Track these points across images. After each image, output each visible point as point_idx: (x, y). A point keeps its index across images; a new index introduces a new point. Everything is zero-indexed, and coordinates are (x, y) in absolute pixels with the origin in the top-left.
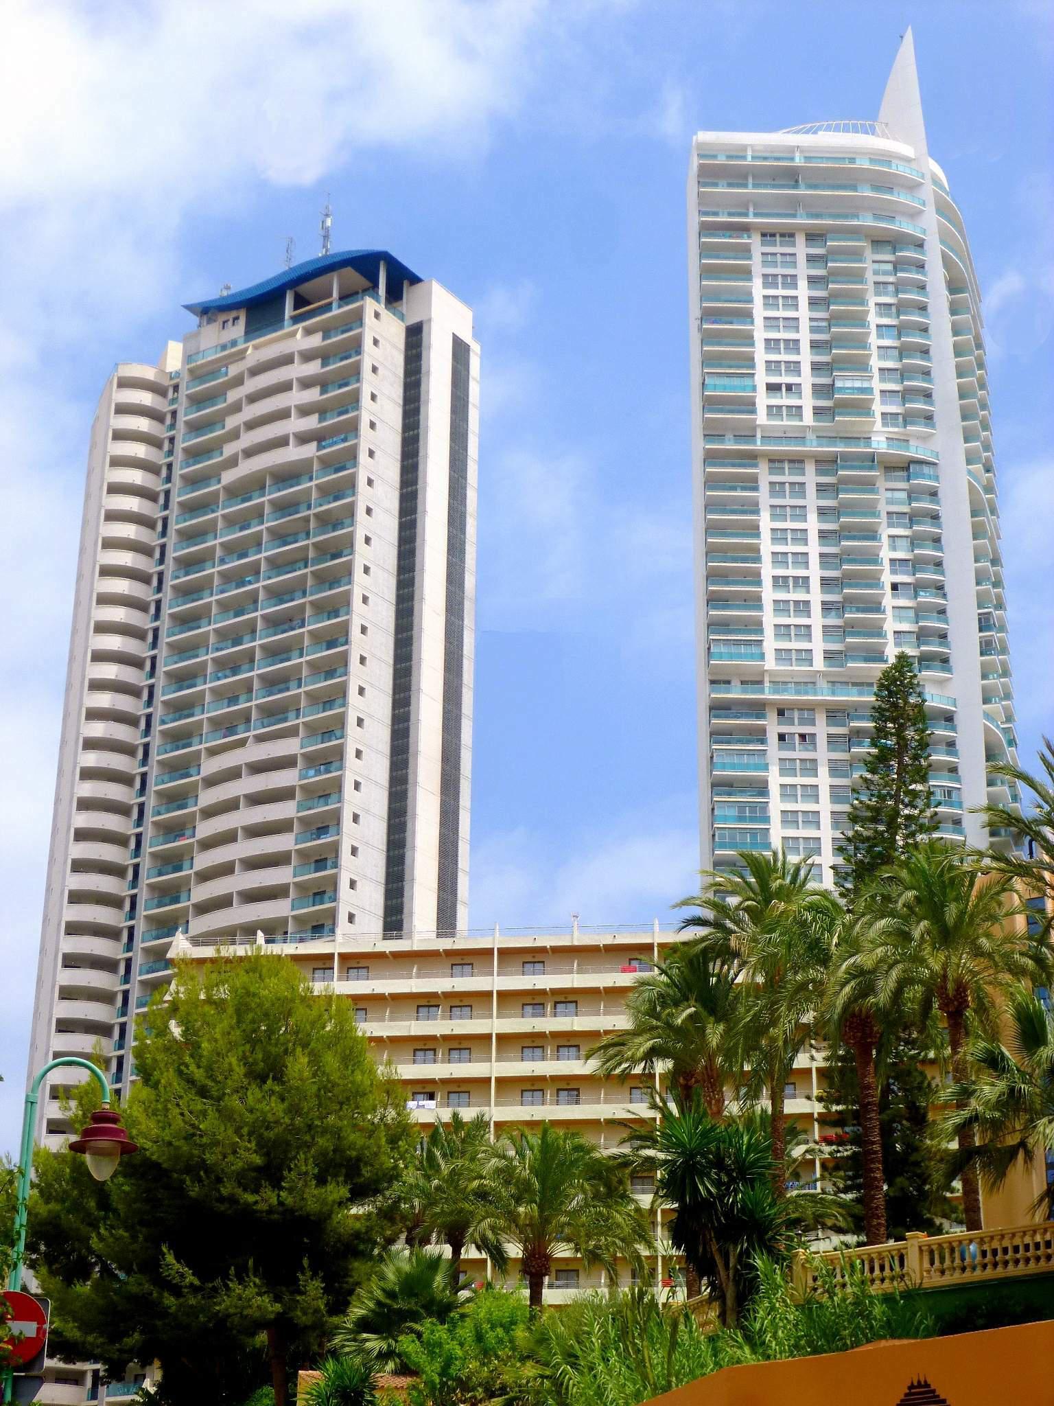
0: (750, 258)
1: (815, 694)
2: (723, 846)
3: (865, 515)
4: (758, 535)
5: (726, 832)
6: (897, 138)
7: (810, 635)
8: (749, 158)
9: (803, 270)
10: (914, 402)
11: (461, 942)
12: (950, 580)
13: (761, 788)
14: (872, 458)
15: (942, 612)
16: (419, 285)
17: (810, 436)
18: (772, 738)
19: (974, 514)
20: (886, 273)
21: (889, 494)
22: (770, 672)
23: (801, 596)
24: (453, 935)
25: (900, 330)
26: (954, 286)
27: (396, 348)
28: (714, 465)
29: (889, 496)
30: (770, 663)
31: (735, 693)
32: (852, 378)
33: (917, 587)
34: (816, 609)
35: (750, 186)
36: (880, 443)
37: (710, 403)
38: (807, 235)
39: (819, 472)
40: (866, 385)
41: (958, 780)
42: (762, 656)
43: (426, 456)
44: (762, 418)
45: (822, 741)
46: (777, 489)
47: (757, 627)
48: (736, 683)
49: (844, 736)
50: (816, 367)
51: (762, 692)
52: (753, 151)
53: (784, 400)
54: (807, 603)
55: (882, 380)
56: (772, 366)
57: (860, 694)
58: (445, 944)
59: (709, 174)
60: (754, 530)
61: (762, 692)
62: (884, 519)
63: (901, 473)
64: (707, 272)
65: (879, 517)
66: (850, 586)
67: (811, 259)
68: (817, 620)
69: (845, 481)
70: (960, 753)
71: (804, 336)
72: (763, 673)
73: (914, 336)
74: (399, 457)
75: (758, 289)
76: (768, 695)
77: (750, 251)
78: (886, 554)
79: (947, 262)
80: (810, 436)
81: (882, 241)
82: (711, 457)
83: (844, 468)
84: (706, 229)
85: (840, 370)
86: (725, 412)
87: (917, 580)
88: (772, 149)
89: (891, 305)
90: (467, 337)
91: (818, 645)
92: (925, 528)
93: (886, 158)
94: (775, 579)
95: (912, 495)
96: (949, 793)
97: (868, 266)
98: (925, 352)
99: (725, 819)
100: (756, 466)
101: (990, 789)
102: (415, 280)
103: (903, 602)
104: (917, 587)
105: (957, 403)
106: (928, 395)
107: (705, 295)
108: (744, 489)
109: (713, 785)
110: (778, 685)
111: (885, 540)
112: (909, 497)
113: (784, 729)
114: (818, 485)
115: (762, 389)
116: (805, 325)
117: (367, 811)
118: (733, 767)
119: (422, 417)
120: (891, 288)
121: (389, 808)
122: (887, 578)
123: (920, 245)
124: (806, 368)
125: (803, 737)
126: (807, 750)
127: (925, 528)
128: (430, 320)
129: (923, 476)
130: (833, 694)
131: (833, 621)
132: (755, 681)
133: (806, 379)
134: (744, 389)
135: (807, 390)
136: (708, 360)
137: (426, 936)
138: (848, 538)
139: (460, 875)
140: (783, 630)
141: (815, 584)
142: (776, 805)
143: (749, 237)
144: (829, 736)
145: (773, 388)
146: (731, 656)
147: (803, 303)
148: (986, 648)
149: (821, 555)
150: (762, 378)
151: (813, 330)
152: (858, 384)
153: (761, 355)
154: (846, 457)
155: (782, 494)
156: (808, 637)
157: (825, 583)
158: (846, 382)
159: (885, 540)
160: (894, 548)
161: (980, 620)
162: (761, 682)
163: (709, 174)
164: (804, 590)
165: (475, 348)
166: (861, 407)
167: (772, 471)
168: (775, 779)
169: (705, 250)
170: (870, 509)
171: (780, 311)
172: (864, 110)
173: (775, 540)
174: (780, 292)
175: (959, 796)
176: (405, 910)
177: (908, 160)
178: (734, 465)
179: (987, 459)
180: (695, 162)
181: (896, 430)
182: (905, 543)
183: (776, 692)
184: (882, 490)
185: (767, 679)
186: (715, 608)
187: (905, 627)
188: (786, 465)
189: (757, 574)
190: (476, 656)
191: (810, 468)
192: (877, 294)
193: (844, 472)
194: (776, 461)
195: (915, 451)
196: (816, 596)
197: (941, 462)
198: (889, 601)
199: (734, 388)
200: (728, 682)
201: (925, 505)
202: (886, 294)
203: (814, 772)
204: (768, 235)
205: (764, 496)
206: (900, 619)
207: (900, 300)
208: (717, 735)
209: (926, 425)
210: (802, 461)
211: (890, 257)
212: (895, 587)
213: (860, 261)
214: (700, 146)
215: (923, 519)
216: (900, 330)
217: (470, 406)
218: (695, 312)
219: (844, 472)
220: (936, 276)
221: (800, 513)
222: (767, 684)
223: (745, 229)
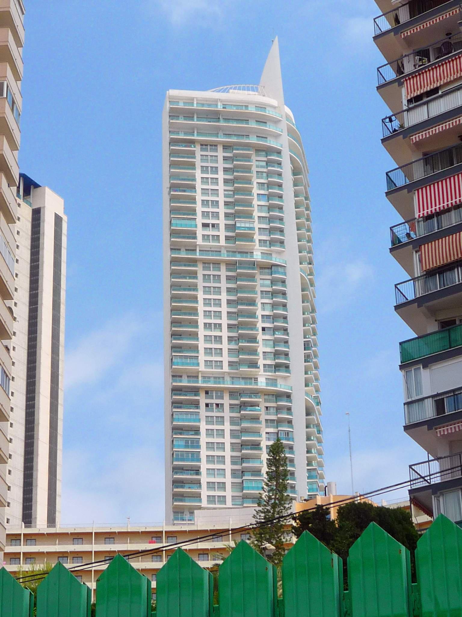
0: (195, 158)
1: (224, 384)
2: (177, 460)
3: (249, 292)
4: (197, 302)
5: (179, 453)
6: (268, 96)
7: (225, 501)
8: (195, 105)
9: (221, 165)
10: (275, 236)
11: (58, 529)
12: (289, 290)
13: (196, 431)
14: (253, 263)
15: (286, 342)
16: (39, 189)
17: (224, 251)
18: (202, 406)
19: (303, 290)
20: (262, 167)
21: (262, 282)
22: (203, 372)
23: (218, 333)
24: (55, 527)
25: (269, 197)
26: (296, 172)
27: (28, 221)
28: (175, 168)
29: (262, 283)
30: (202, 368)
31: (185, 383)
33: (275, 329)
34: (225, 340)
36: (257, 256)
37: (174, 233)
38: (223, 146)
39: (228, 270)
40: (251, 226)
41: (292, 428)
42: (198, 364)
43: (40, 348)
44: (199, 241)
45: (227, 408)
46: (206, 278)
47: (195, 348)
48: (183, 250)
49: (238, 405)
50: (227, 215)
51: (198, 382)
52: (197, 100)
53: (210, 232)
54: (220, 337)
55: (260, 223)
56: (205, 214)
57: (246, 384)
58: (52, 530)
59: (174, 114)
60: (195, 299)
61: (198, 382)
62: (259, 295)
63: (267, 271)
64: (173, 165)
65: (252, 173)
66: (242, 329)
67: (225, 159)
68: (225, 346)
69: (240, 275)
70: (291, 372)
71: (221, 199)
72: (198, 372)
73: (275, 200)
74: (29, 276)
75: (199, 174)
76: (200, 384)
77: (194, 154)
78: (260, 312)
79: (292, 160)
80: (224, 251)
81: (259, 150)
82: (174, 261)
83: (240, 268)
84: (173, 142)
85: (239, 217)
86: (181, 238)
87: (275, 326)
88: (206, 100)
89: (274, 420)
90: (61, 214)
91: (225, 358)
92: (279, 299)
93: (262, 107)
94: (204, 236)
95: (273, 282)
96: (288, 433)
97: (254, 163)
98: (281, 208)
99: (179, 446)
100: (196, 266)
101: (308, 430)
102: (37, 186)
103: (267, 337)
104: (275, 329)
105: (300, 293)
106: (281, 231)
107: (172, 176)
108: (190, 278)
109: (172, 348)
110: (206, 378)
111: (259, 305)
112: (272, 283)
113: (209, 401)
114: (224, 179)
115: (200, 226)
116: (221, 193)
117: (15, 452)
118: (183, 420)
119: (34, 464)
120: (265, 175)
121: (24, 482)
122: (260, 325)
123: (279, 152)
124: (222, 216)
125: (217, 405)
126: (220, 412)
127: (279, 299)
128: (44, 207)
129: (279, 273)
130: (233, 384)
131: (233, 346)
132: (194, 376)
133: (222, 222)
134: (191, 226)
135: (222, 227)
136: (173, 210)
137: (42, 527)
138: (242, 305)
139: (59, 436)
140: (210, 419)
141: (225, 327)
142: (204, 439)
143: (195, 147)
144: (230, 405)
145: (205, 225)
146: (183, 364)
147: (221, 182)
148: (307, 358)
149: (228, 313)
150: (200, 220)
151: (226, 196)
152: (247, 225)
153: (199, 208)
154: (241, 262)
155: (207, 160)
156: (221, 354)
157: (230, 327)
158: (242, 224)
159: (259, 305)
160: (263, 309)
161: (305, 344)
162: (197, 377)
163: (174, 114)
164: (219, 330)
165: (65, 218)
166: (249, 238)
167: (204, 268)
168: (203, 427)
169: (173, 153)
170: (252, 289)
171: (210, 186)
172: (251, 78)
173: (205, 304)
174: (210, 176)
175: (293, 435)
176: (33, 500)
177: (275, 108)
178: (185, 266)
179: (308, 215)
180: (168, 106)
181: (270, 374)
182: (269, 307)
183: (204, 382)
184: (258, 280)
185: (200, 375)
186: (175, 339)
187: (268, 350)
188: (211, 266)
189: (196, 322)
190: (66, 316)
191: (223, 267)
192: (258, 178)
193: (241, 271)
194: (206, 264)
195: (276, 260)
196: (225, 333)
197: (288, 266)
198: (261, 337)
199: (186, 226)
200: (180, 250)
201: (279, 288)
202: (262, 178)
203: (223, 423)
204: (204, 145)
205: (200, 282)
206: (266, 346)
207: (269, 181)
208: (176, 404)
209: (281, 247)
210: (219, 264)
211: (265, 159)
212: (264, 329)
213: (249, 161)
214: (170, 97)
215: (278, 294)
216: (269, 197)
217: (63, 235)
218: (166, 184)
219: (241, 271)
220: (287, 169)
221: (218, 290)
222: (200, 378)
223: (194, 262)
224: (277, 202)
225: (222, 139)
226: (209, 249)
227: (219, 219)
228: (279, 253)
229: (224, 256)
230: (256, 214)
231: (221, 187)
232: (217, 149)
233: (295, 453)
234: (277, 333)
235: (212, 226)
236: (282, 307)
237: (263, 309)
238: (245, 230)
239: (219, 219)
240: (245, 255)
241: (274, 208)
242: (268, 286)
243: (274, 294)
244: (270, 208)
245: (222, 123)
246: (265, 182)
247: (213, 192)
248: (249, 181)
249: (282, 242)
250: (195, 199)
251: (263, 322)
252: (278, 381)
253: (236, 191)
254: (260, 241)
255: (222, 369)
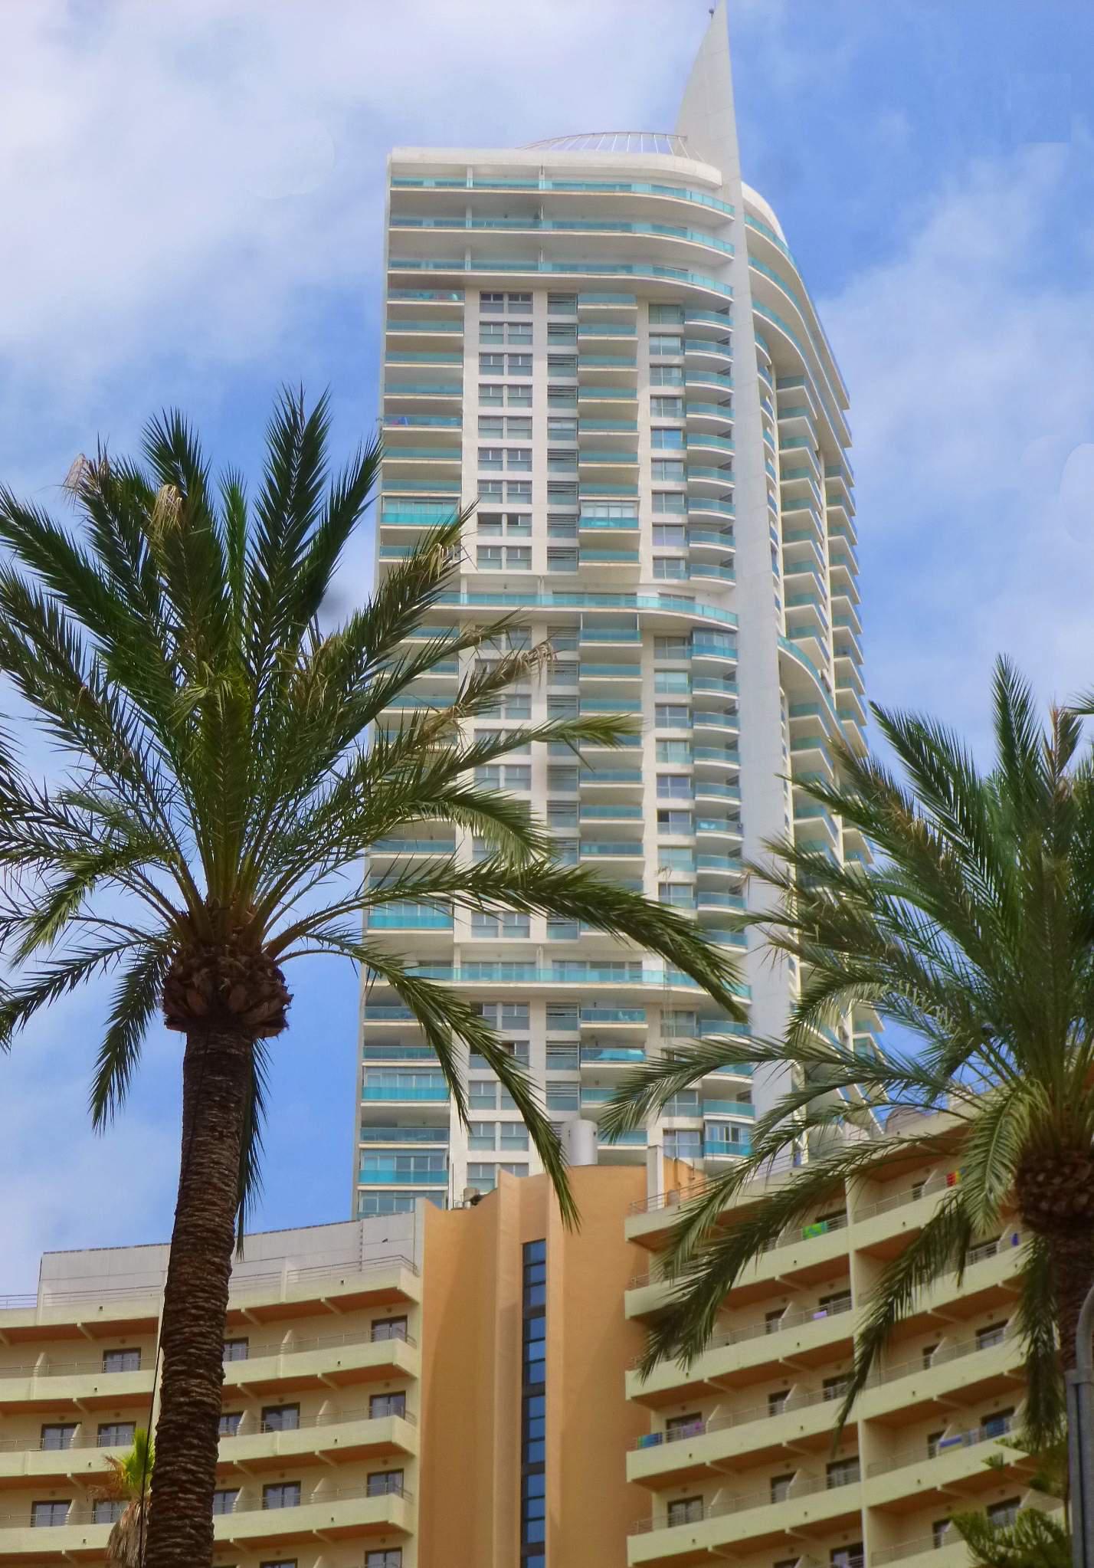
8: (469, 184)
9: (541, 347)
14: (630, 621)
20: (669, 351)
22: (465, 948)
29: (658, 681)
32: (608, 505)
33: (700, 815)
35: (469, 223)
38: (550, 296)
40: (629, 514)
50: (556, 490)
53: (504, 537)
67: (554, 330)
71: (540, 444)
75: (472, 374)
79: (762, 332)
89: (678, 559)
96: (735, 1132)
104: (700, 815)
116: (540, 426)
122: (652, 802)
123: (723, 310)
129: (712, 650)
130: (562, 981)
133: (540, 507)
135: (540, 523)
152: (615, 513)
158: (599, 513)
166: (623, 547)
177: (713, 188)
181: (675, 581)
185: (457, 958)
195: (706, 613)
198: (652, 836)
204: (491, 297)
212: (663, 816)
215: (709, 714)
223: (457, 286)
224: (715, 448)
225: (546, 273)
226: (501, 590)
227: (530, 502)
228: (720, 594)
229: (546, 980)
230: (647, 483)
231: (540, 409)
232: (529, 710)
233: (741, 689)
234: (704, 825)
235: (509, 522)
236: (727, 895)
237: (664, 757)
238: (607, 527)
239: (530, 502)
240: (612, 971)
241: (704, 467)
242: (681, 691)
243: (697, 711)
244: (691, 465)
245: (547, 230)
246: (680, 554)
247: (515, 425)
248: (627, 387)
249: (726, 564)
250: (459, 445)
251: (662, 793)
252: (698, 600)
253: (588, 416)
254: (662, 778)
255: (527, 935)
